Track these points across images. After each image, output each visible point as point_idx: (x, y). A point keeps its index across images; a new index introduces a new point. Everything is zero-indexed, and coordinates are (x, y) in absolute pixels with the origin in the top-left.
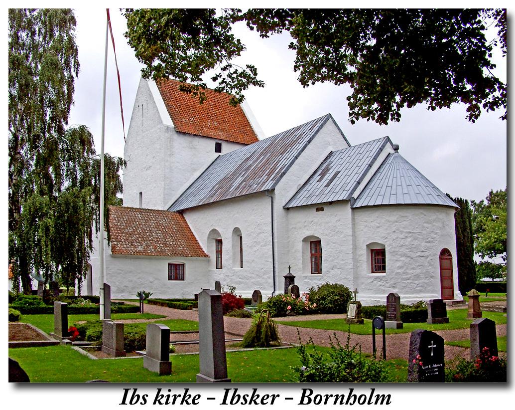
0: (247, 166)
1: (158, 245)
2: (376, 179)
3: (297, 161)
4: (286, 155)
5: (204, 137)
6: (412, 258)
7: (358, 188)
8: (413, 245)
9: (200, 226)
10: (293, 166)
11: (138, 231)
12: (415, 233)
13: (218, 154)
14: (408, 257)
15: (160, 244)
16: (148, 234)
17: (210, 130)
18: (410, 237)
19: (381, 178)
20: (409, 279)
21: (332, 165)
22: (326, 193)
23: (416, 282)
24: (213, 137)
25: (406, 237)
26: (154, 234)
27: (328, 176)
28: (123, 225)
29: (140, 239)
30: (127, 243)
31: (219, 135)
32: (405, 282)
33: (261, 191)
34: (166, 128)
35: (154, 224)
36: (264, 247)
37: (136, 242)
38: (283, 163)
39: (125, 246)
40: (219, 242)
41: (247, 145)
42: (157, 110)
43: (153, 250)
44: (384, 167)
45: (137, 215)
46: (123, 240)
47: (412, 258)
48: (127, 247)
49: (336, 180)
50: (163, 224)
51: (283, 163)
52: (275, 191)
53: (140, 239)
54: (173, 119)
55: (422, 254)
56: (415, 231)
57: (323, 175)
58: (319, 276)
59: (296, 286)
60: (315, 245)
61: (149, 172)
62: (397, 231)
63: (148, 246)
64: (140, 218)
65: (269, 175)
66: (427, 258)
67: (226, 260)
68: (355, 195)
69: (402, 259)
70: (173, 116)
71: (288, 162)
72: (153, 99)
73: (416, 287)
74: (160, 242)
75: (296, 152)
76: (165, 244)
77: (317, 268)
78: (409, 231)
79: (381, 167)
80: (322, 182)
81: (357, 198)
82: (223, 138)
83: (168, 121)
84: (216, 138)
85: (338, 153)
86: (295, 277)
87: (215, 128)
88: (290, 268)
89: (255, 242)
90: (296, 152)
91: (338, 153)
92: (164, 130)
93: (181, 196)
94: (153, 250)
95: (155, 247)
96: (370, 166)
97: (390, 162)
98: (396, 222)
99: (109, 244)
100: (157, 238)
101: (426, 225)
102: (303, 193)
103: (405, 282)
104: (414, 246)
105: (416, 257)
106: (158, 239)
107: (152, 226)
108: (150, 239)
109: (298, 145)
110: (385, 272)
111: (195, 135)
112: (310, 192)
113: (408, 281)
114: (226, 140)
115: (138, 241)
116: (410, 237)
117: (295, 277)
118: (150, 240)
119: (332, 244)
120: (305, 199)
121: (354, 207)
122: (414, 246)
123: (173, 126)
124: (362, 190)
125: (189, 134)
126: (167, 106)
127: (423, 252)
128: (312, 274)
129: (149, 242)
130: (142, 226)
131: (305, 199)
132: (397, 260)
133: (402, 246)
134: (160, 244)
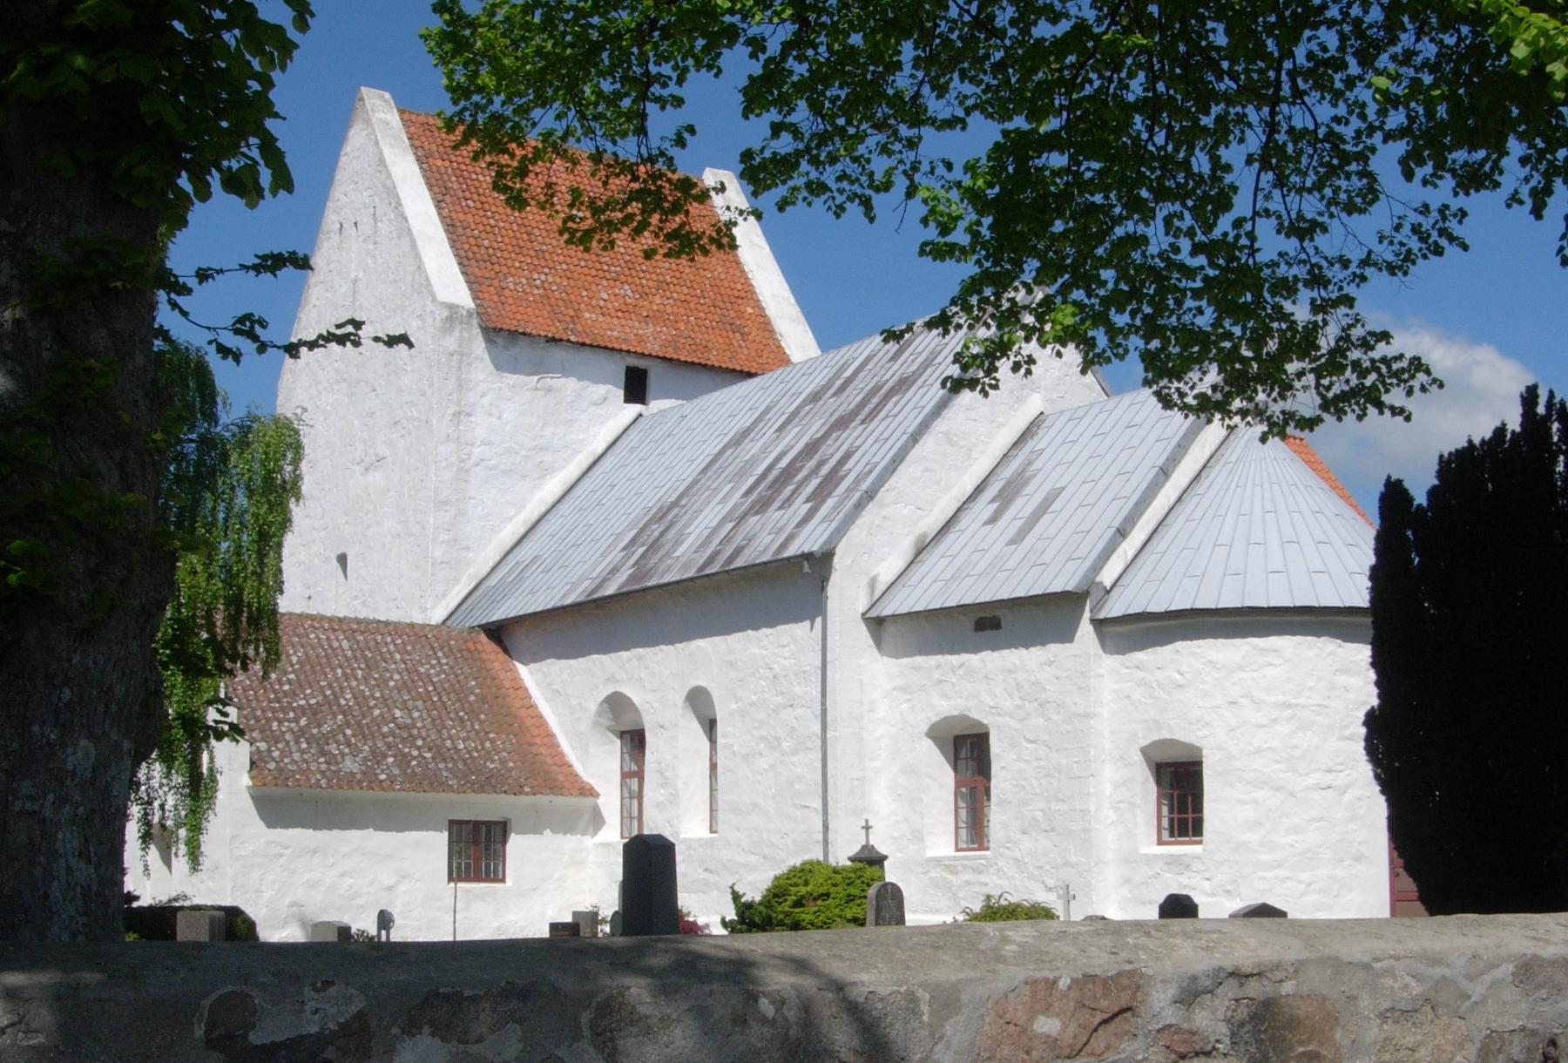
0: (738, 464)
1: (415, 753)
2: (1182, 519)
3: (916, 452)
4: (878, 426)
5: (584, 344)
6: (1292, 794)
7: (1120, 551)
8: (1296, 747)
9: (561, 695)
10: (902, 468)
11: (343, 702)
12: (1304, 707)
13: (636, 408)
14: (1278, 789)
15: (419, 748)
16: (377, 712)
17: (609, 319)
18: (1288, 719)
19: (1197, 515)
20: (1279, 866)
21: (1037, 465)
22: (1011, 564)
23: (1305, 876)
24: (617, 346)
25: (1275, 720)
26: (398, 713)
27: (1023, 506)
28: (289, 682)
29: (348, 732)
30: (304, 746)
31: (641, 339)
32: (1265, 874)
33: (788, 559)
34: (445, 313)
35: (396, 677)
36: (794, 759)
37: (338, 742)
38: (868, 456)
39: (296, 756)
40: (635, 740)
41: (750, 375)
42: (414, 246)
43: (396, 771)
44: (1212, 476)
45: (335, 644)
46: (288, 737)
47: (1292, 794)
48: (306, 761)
49: (1046, 518)
50: (429, 676)
51: (868, 456)
52: (836, 559)
53: (348, 732)
54: (417, 143)
55: (1327, 779)
56: (1302, 701)
57: (1006, 497)
58: (981, 858)
59: (893, 885)
60: (968, 749)
61: (375, 478)
62: (1243, 701)
63: (377, 756)
64: (349, 654)
65: (819, 497)
66: (1344, 793)
67: (658, 805)
68: (1107, 577)
69: (1259, 794)
70: (469, 270)
71: (884, 457)
72: (399, 204)
73: (1304, 893)
74: (420, 743)
75: (911, 416)
76: (440, 755)
77: (975, 829)
78: (1282, 699)
79: (1204, 474)
80: (1002, 523)
81: (1114, 586)
82: (653, 347)
83: (452, 287)
84: (628, 352)
85: (1064, 419)
86: (886, 857)
87: (625, 312)
88: (867, 828)
89: (763, 738)
90: (911, 416)
91: (1064, 419)
92: (438, 324)
93: (494, 569)
94: (396, 771)
95: (403, 760)
96: (1165, 472)
97: (1234, 458)
98: (1241, 668)
99: (1396, 411)
100: (406, 727)
101: (1342, 680)
102: (934, 563)
103: (1265, 874)
104: (1297, 753)
105: (1308, 789)
106: (415, 732)
107: (392, 684)
108: (385, 729)
109: (921, 392)
110: (1200, 843)
111: (553, 340)
112: (958, 562)
113: (1279, 873)
114: (664, 358)
115: (340, 737)
116: (1288, 719)
117: (886, 857)
118: (384, 736)
119: (1025, 744)
120: (939, 585)
121: (1101, 616)
122: (1297, 753)
123: (473, 305)
124: (1130, 555)
125: (530, 335)
126: (450, 227)
127: (1330, 771)
128: (958, 850)
129: (380, 744)
130: (354, 683)
131: (939, 585)
132: (1240, 801)
133: (1258, 751)
134: (419, 748)
